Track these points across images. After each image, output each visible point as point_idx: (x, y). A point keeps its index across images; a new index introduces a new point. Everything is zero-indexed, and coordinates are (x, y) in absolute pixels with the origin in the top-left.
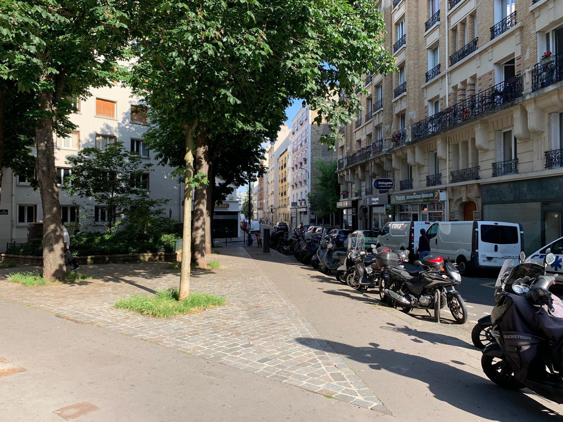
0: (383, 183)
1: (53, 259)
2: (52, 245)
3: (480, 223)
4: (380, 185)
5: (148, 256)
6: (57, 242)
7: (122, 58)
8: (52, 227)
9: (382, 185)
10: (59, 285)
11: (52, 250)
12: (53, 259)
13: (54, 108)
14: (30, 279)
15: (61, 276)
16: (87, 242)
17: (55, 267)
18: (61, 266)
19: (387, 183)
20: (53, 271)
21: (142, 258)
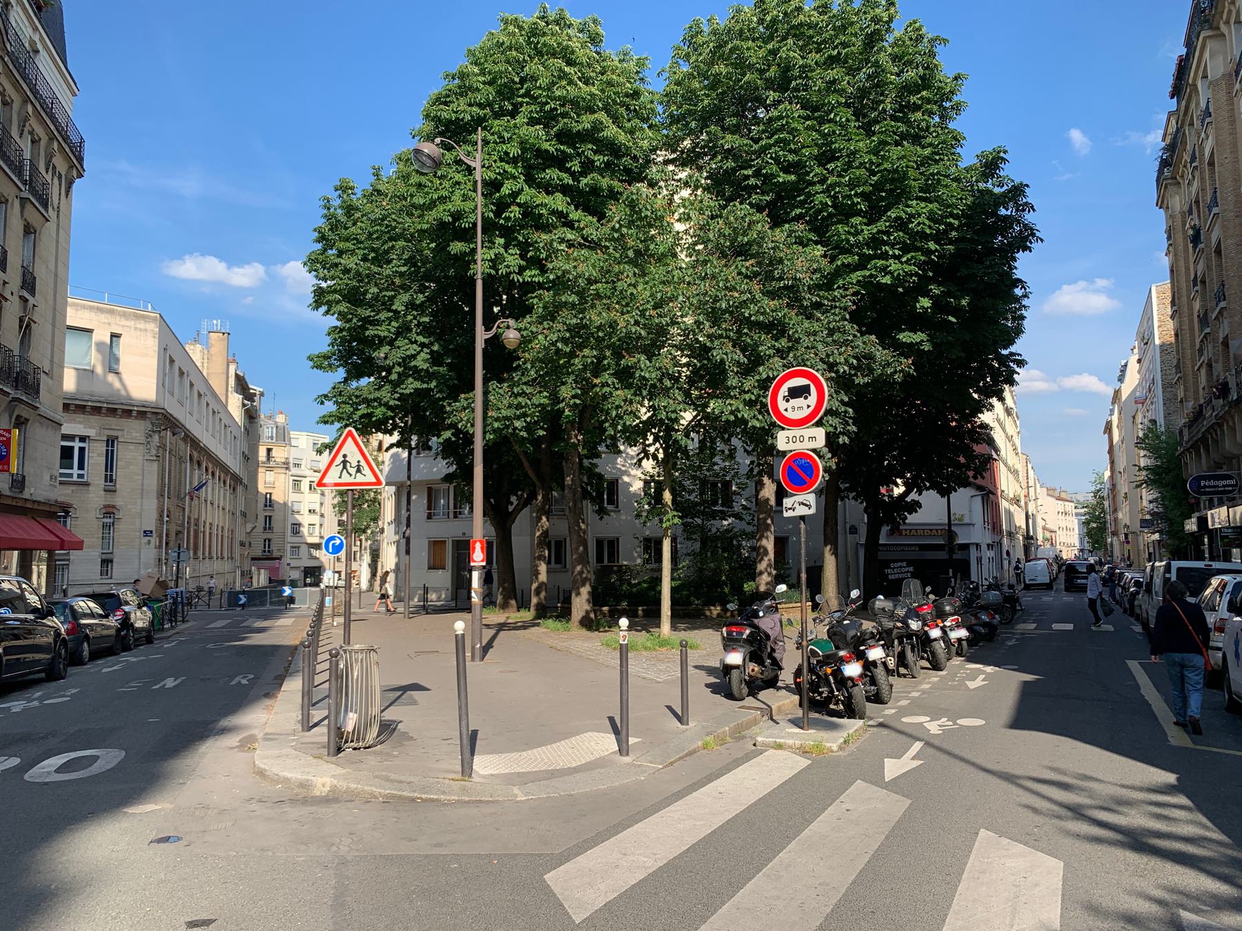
0: (1212, 483)
1: (581, 604)
2: (578, 588)
3: (1176, 564)
4: (1205, 486)
5: (716, 611)
6: (583, 585)
7: (58, 634)
8: (579, 568)
9: (1210, 487)
10: (584, 632)
11: (578, 594)
12: (581, 604)
13: (580, 437)
14: (558, 624)
15: (588, 624)
16: (648, 589)
17: (582, 614)
18: (587, 612)
19: (1222, 483)
20: (579, 618)
21: (708, 613)
